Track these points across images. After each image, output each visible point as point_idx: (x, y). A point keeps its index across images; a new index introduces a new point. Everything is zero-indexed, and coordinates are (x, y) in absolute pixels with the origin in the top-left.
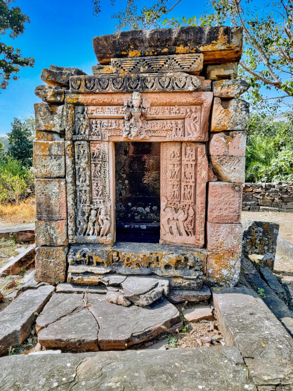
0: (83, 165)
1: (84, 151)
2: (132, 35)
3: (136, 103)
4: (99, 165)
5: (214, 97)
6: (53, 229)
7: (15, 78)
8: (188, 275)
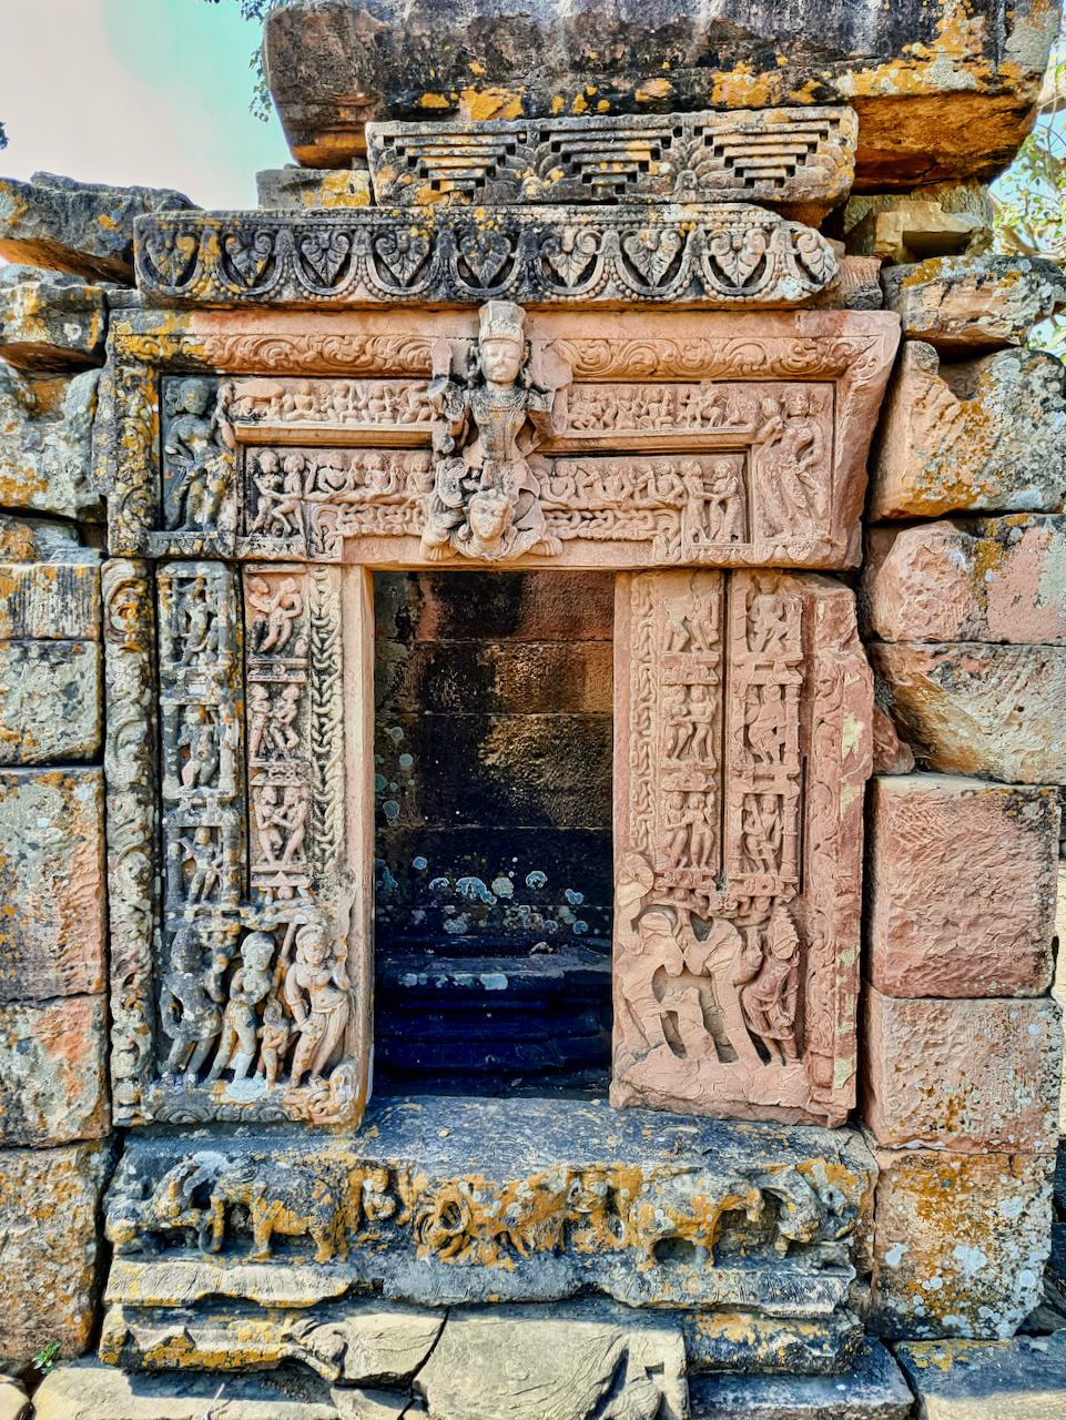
0: (204, 690)
1: (210, 616)
3: (498, 359)
4: (291, 693)
6: (23, 1051)
8: (786, 1298)
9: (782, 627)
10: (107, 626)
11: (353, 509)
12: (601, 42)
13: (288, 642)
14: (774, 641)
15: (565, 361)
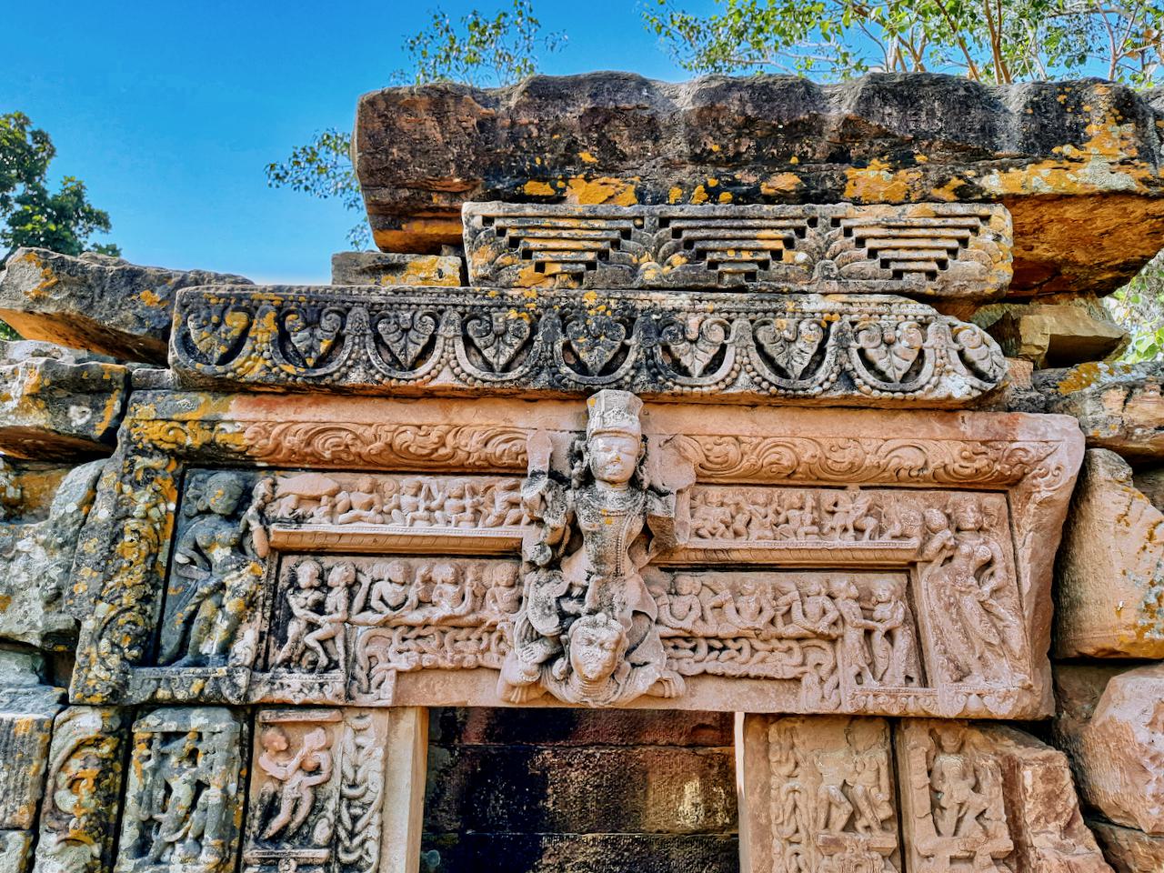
1: (199, 787)
2: (593, 96)
5: (1091, 444)
9: (977, 801)
10: (47, 806)
11: (413, 634)
12: (725, 135)
13: (305, 821)
14: (969, 819)
15: (687, 459)
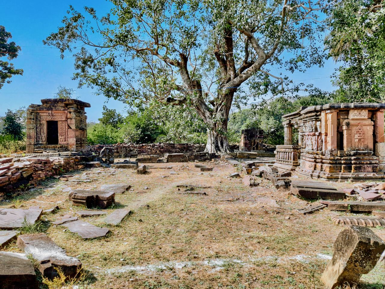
7: (8, 82)
